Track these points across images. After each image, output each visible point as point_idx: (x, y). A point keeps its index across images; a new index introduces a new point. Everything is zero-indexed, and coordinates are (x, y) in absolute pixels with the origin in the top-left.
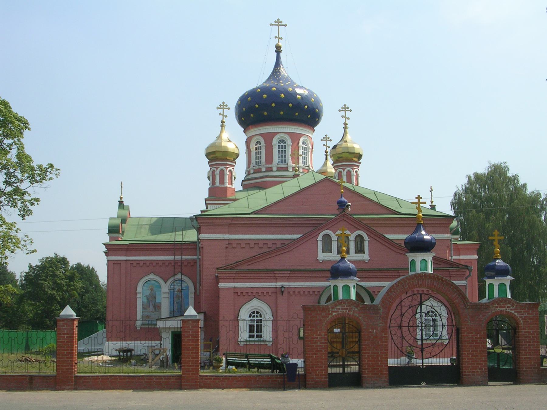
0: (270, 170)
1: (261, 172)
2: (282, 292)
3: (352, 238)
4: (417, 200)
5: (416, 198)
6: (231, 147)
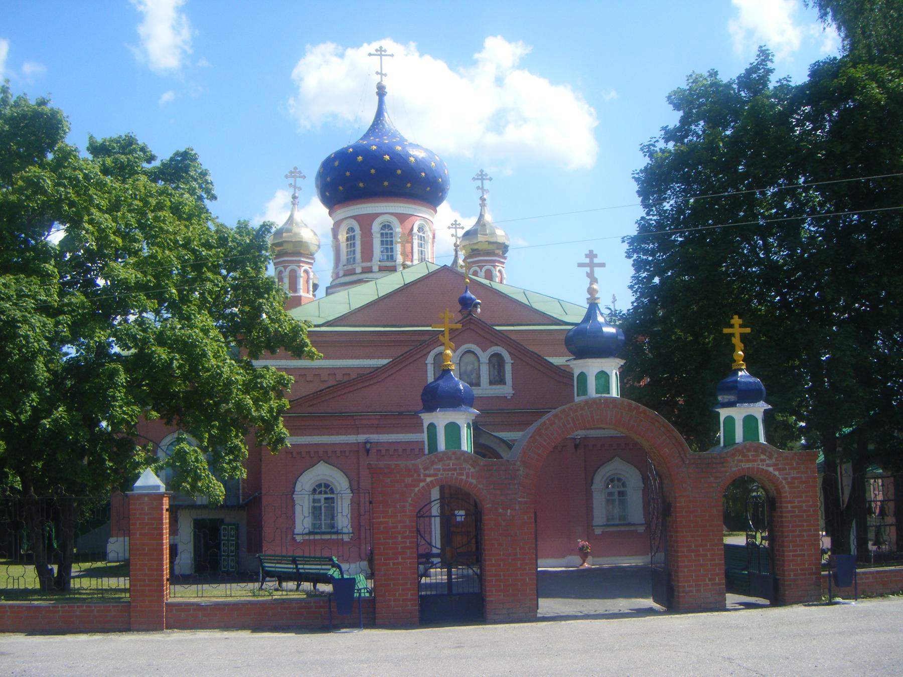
1: (355, 274)
2: (368, 451)
3: (484, 357)
4: (587, 261)
5: (587, 256)
6: (306, 235)
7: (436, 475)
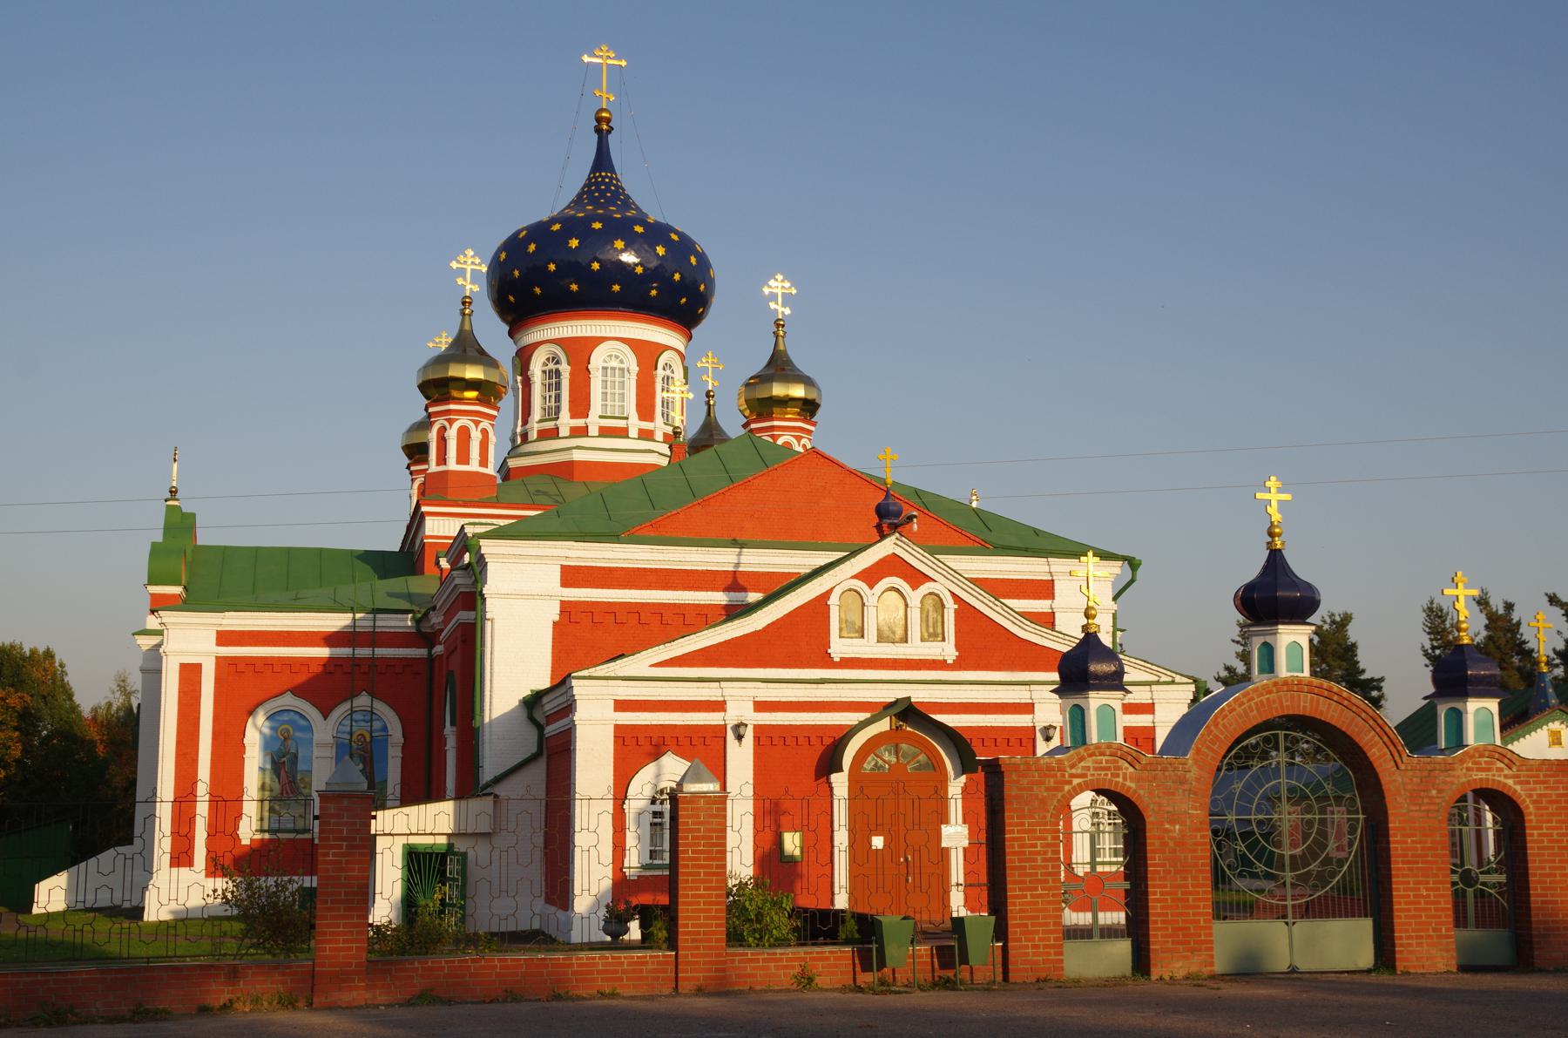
0: (581, 432)
7: (1084, 776)
